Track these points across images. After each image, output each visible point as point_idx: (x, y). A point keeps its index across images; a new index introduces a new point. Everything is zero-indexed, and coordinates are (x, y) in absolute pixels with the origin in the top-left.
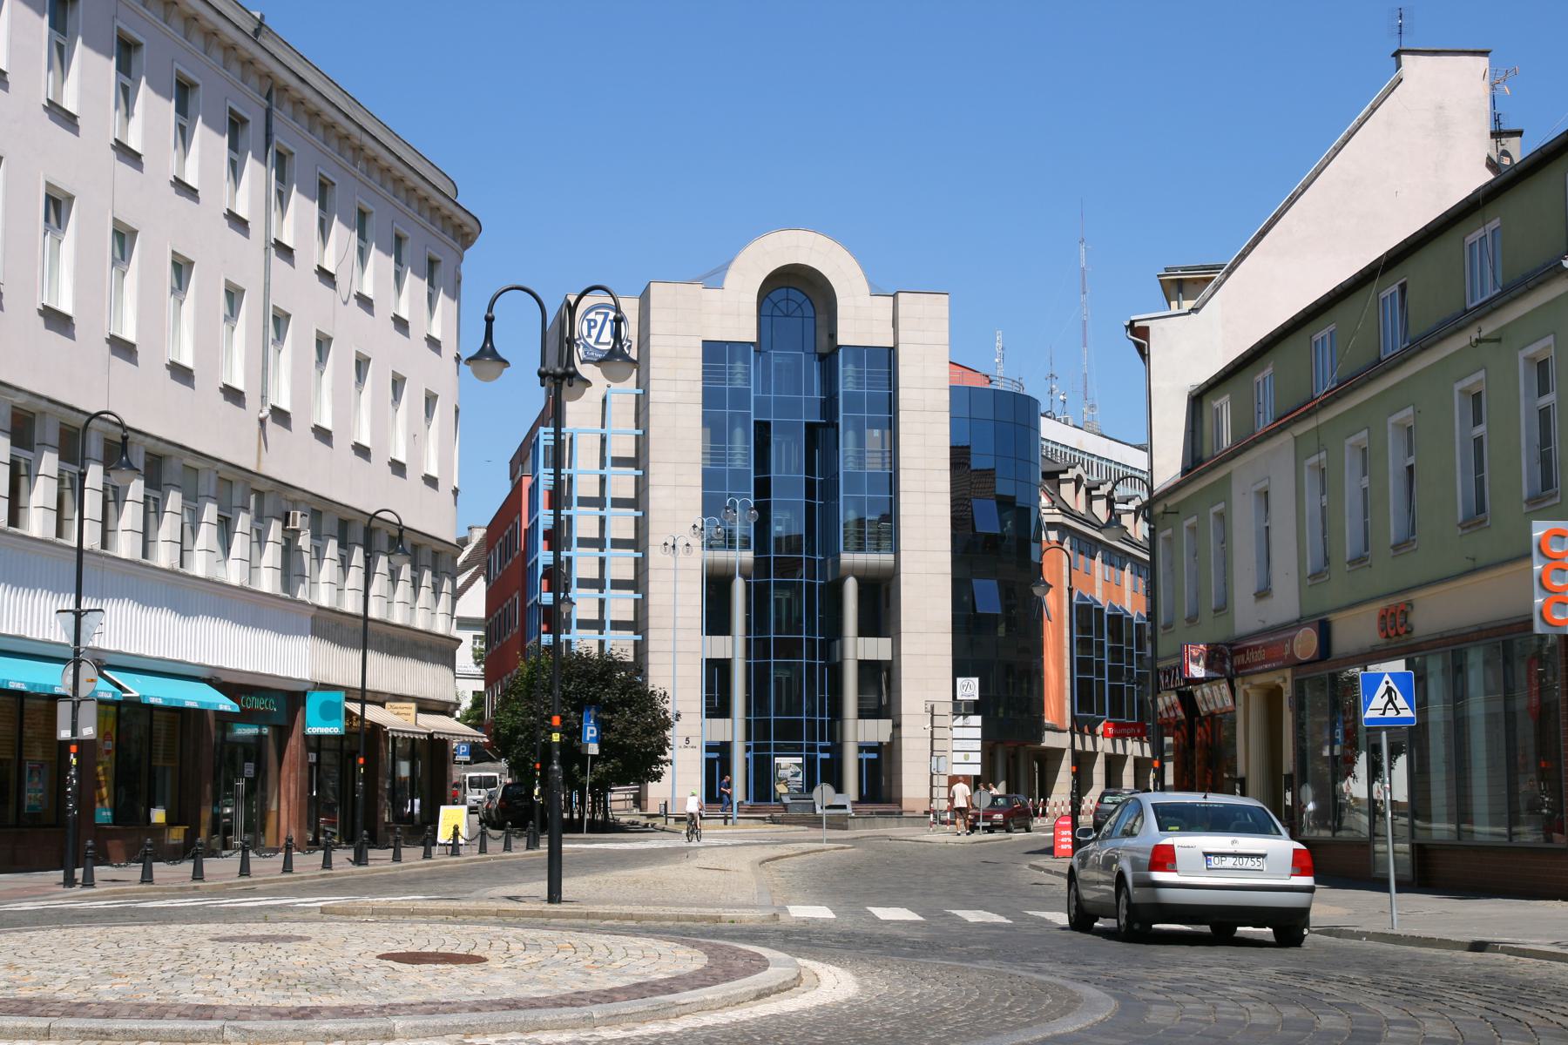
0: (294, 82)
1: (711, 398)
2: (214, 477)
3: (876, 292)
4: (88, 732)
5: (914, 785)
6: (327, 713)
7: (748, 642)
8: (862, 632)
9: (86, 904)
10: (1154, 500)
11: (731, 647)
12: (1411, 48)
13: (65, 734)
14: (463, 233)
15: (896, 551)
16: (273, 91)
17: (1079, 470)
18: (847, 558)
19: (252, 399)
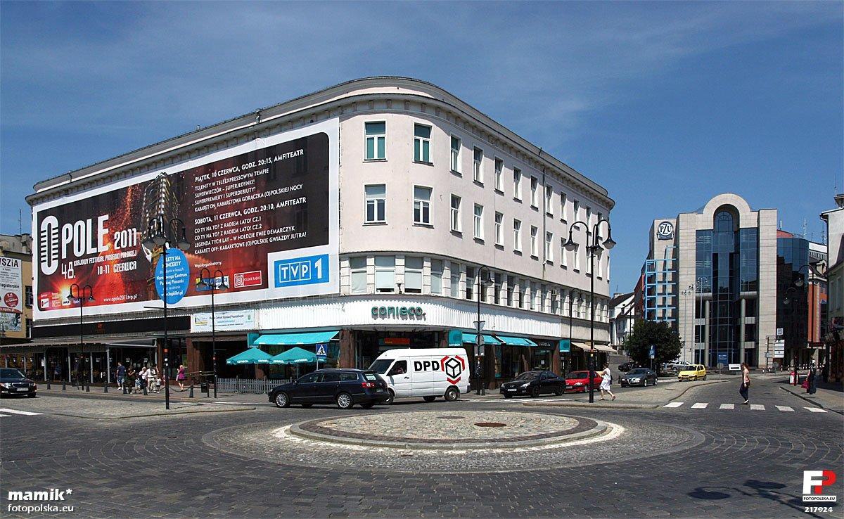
0: (551, 166)
1: (698, 247)
2: (529, 282)
3: (752, 211)
4: (482, 354)
5: (762, 361)
6: (565, 347)
7: (710, 320)
8: (747, 316)
9: (666, 381)
10: (828, 270)
11: (704, 322)
12: (306, 94)
13: (477, 355)
14: (610, 205)
15: (758, 290)
16: (545, 169)
17: (824, 261)
18: (742, 293)
19: (541, 259)
